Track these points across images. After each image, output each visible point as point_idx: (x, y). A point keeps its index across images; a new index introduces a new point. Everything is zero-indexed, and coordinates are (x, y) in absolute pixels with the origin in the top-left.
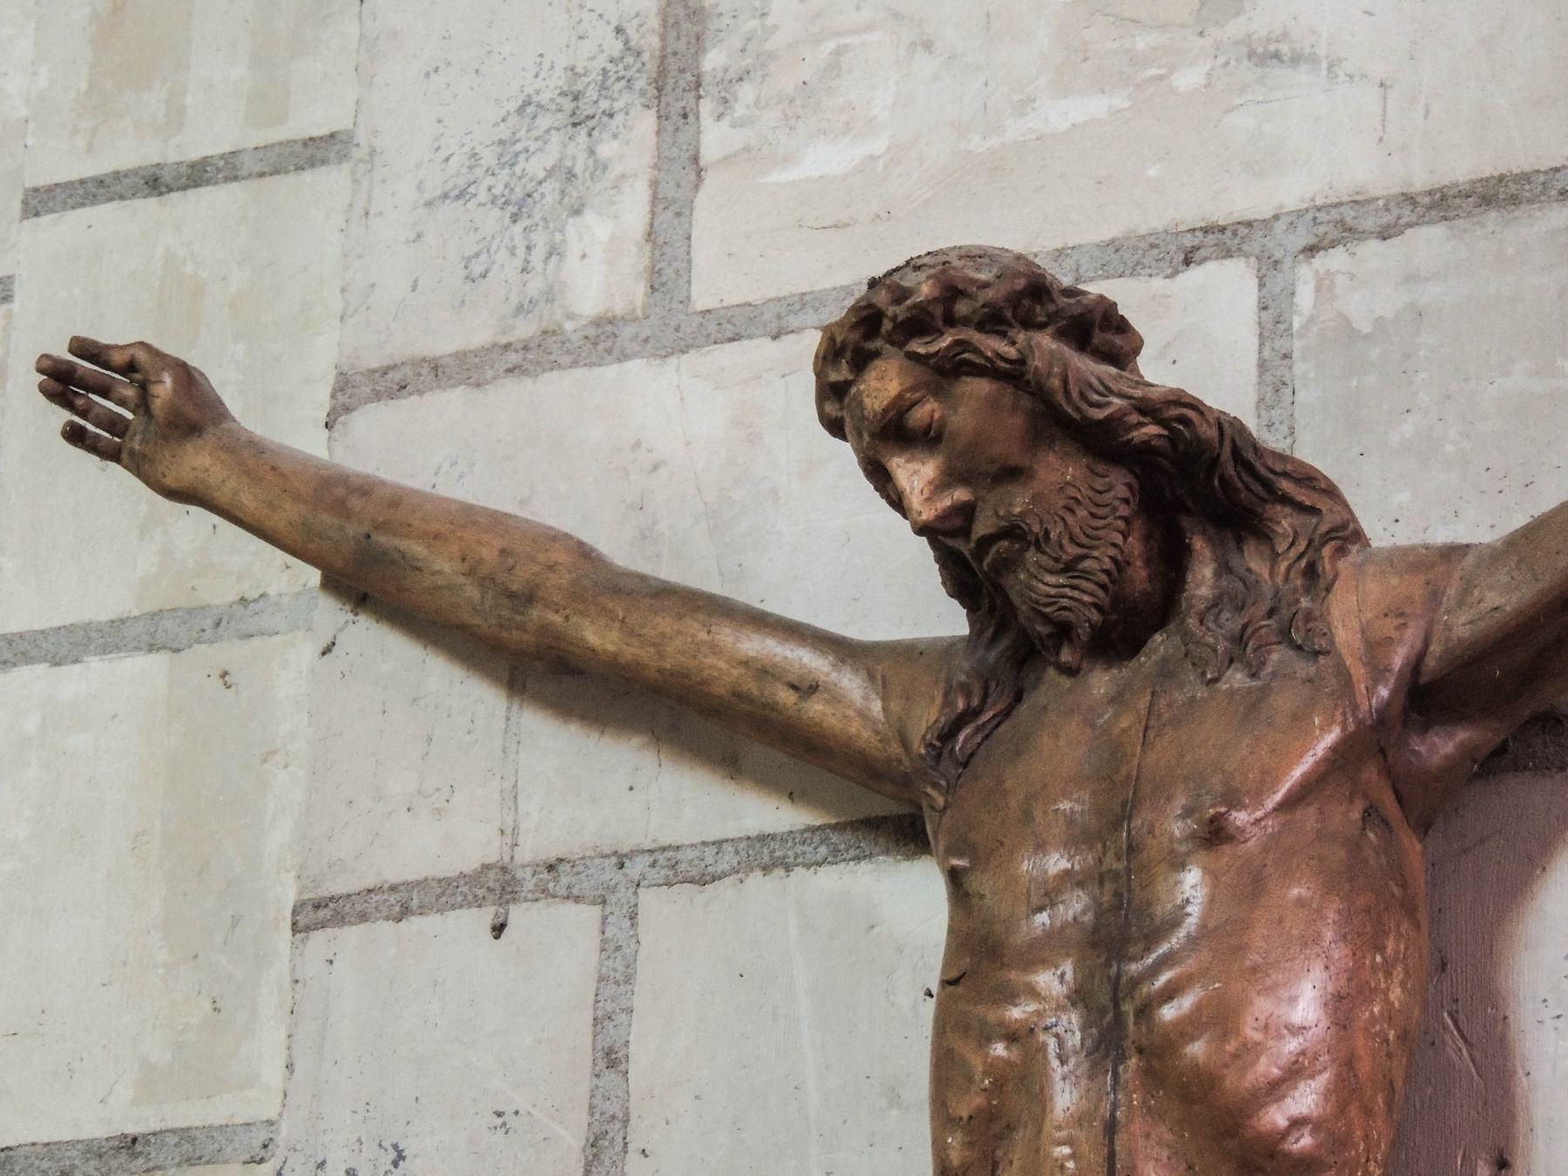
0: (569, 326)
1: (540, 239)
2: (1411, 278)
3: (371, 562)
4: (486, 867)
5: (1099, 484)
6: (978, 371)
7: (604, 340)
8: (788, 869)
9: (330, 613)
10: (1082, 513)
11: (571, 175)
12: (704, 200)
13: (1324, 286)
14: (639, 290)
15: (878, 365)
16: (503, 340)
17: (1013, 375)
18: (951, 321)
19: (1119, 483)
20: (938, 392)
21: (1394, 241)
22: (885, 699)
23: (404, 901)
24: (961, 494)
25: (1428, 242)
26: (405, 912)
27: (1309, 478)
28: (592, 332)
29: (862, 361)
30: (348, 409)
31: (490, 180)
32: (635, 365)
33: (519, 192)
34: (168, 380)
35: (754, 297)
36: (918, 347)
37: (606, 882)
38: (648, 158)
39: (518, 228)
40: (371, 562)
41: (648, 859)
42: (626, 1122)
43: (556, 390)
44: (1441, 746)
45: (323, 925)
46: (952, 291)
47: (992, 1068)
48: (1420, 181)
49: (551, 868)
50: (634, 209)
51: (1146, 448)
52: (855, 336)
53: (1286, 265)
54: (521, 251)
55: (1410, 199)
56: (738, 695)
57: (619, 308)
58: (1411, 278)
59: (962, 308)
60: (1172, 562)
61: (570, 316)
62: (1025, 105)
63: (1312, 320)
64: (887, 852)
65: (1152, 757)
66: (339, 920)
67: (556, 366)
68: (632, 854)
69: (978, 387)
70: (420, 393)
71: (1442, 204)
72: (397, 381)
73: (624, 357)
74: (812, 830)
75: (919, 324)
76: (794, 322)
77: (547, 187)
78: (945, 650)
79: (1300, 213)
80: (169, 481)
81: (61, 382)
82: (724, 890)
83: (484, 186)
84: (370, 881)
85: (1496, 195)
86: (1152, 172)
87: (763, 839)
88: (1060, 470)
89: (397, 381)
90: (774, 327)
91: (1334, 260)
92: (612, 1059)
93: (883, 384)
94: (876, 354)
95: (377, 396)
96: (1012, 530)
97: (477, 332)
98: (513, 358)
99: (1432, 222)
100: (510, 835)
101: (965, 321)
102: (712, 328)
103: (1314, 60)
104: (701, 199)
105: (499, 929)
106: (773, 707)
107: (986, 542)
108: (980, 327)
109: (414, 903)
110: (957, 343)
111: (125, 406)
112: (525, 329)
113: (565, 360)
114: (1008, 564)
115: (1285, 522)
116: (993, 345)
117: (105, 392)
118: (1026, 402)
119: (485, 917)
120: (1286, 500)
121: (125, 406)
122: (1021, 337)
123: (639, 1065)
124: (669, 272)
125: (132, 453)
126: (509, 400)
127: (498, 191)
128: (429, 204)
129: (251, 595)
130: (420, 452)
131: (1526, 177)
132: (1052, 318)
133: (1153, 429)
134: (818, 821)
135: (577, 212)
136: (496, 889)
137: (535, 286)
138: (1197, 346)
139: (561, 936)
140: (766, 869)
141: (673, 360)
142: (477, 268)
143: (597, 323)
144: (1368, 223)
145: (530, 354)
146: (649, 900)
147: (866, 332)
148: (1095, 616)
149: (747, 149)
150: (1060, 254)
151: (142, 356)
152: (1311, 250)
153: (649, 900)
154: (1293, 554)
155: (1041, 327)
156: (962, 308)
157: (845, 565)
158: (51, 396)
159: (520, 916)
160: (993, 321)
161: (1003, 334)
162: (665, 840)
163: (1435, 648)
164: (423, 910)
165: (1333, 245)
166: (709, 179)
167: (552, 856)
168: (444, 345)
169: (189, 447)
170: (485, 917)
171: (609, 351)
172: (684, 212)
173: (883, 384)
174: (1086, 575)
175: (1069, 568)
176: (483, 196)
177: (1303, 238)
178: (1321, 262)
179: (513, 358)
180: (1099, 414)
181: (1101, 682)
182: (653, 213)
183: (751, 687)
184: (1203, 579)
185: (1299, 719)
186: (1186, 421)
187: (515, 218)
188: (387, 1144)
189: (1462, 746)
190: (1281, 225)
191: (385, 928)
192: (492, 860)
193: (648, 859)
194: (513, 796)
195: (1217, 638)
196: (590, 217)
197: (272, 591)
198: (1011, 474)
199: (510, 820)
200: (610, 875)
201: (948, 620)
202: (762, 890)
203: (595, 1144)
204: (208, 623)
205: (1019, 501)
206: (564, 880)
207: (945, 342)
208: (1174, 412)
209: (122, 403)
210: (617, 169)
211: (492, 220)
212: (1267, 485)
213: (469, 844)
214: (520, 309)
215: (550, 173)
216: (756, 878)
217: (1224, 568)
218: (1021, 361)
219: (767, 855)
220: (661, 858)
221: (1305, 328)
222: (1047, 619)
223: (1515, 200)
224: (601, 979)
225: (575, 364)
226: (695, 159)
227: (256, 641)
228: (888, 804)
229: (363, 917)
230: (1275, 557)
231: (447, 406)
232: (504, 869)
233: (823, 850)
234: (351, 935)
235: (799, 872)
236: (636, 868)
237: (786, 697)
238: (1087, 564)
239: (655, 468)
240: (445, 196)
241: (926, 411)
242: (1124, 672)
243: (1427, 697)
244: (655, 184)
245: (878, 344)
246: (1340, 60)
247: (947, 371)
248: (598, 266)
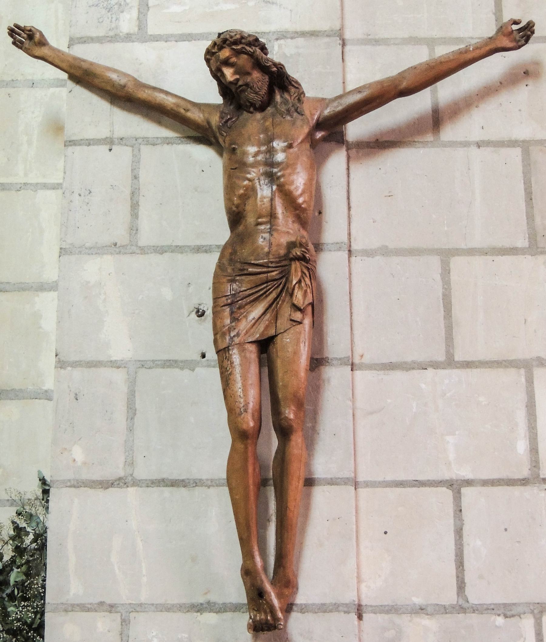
0: (121, 34)
1: (114, 16)
2: (297, 47)
3: (84, 76)
4: (107, 138)
5: (263, 78)
6: (246, 53)
7: (128, 38)
8: (172, 144)
9: (71, 84)
10: (260, 83)
11: (120, 5)
12: (149, 13)
13: (280, 46)
14: (136, 29)
15: (225, 49)
16: (107, 35)
17: (251, 55)
18: (241, 43)
19: (267, 78)
20: (236, 56)
21: (294, 40)
22: (203, 114)
23: (89, 143)
24: (238, 77)
25: (300, 41)
26: (89, 145)
27: (297, 82)
28: (126, 36)
29: (221, 48)
30: (73, 45)
31: (103, 4)
32: (136, 43)
33: (109, 7)
34: (38, 33)
35: (162, 33)
36: (234, 47)
37: (134, 143)
38: (137, 4)
39: (109, 14)
40: (84, 76)
41: (142, 140)
42: (139, 189)
43: (119, 46)
44: (319, 135)
45: (71, 145)
46: (242, 38)
47: (245, 186)
48: (299, 29)
49: (121, 139)
50: (135, 13)
51: (273, 72)
52: (221, 43)
53: (272, 41)
54: (110, 18)
55: (296, 32)
56: (172, 109)
57: (132, 32)
58: (297, 47)
59: (243, 41)
60: (271, 93)
61: (121, 32)
62: (218, 4)
63: (278, 52)
64: (193, 143)
65: (276, 130)
66: (75, 145)
67: (118, 42)
68: (139, 138)
69: (245, 56)
70: (88, 43)
71: (303, 34)
72: (84, 40)
73: (133, 42)
74: (177, 137)
75: (236, 43)
76: (169, 39)
77: (116, 6)
78: (218, 106)
79: (275, 32)
80: (36, 54)
81: (12, 32)
82: (158, 147)
83: (102, 5)
84: (82, 138)
85: (313, 34)
86: (244, 20)
87: (167, 138)
88: (256, 75)
89: (84, 40)
90: (165, 40)
91: (282, 42)
92: (136, 177)
93: (225, 53)
94: (225, 47)
95: (79, 43)
96: (247, 85)
97: (101, 33)
98: (109, 39)
99: (301, 37)
100: (112, 132)
101: (243, 44)
102: (152, 38)
103: (276, 4)
104: (149, 13)
105: (110, 150)
106: (179, 113)
107: (241, 86)
108: (247, 45)
109: (91, 143)
110: (243, 47)
111: (26, 39)
112: (111, 34)
113: (121, 41)
114: (243, 91)
115: (293, 90)
116: (248, 48)
117: (19, 35)
118: (252, 60)
119: (107, 147)
120: (293, 86)
121: (26, 39)
122: (254, 48)
123: (141, 180)
124: (143, 26)
125: (26, 48)
126: (108, 48)
127: (105, 6)
128: (90, 6)
129: (15, 79)
130: (90, 54)
131: (320, 32)
132: (259, 45)
133: (275, 69)
134: (180, 136)
135: (122, 12)
136: (110, 142)
137: (113, 25)
138: (277, 53)
139: (124, 154)
140: (168, 144)
141: (144, 44)
142: (101, 20)
143: (127, 34)
144: (288, 36)
145: (114, 39)
146: (142, 147)
147: (225, 41)
148: (260, 102)
149: (158, 5)
150: (496, 26)
151: (33, 29)
152: (277, 39)
153: (142, 147)
154: (295, 95)
155: (256, 46)
156: (243, 41)
157: (199, 88)
158: (9, 34)
159: (114, 148)
160: (250, 44)
161: (250, 47)
162: (145, 136)
163: (321, 117)
164: (93, 145)
165: (281, 39)
166: (151, 10)
167: (121, 137)
168: (94, 35)
169: (42, 48)
170: (108, 147)
171: (130, 40)
172: (145, 15)
173: (225, 53)
174: (259, 95)
175: (256, 93)
176: (101, 6)
177: (275, 37)
178: (279, 42)
179: (109, 39)
180: (268, 65)
181: (258, 116)
182: (139, 14)
183: (175, 109)
184: (278, 98)
185: (302, 126)
186: (281, 68)
187: (109, 11)
188: (87, 189)
189: (322, 136)
190: (271, 34)
191: (85, 148)
192: (108, 136)
193: (142, 140)
194: (112, 124)
195: (283, 108)
196: (125, 13)
197: (19, 79)
198: (249, 74)
199: (112, 129)
200: (134, 142)
201: (219, 100)
202: (166, 147)
203: (133, 193)
204: (5, 84)
205: (249, 79)
206: (124, 142)
207: (239, 47)
208: (280, 66)
209: (23, 38)
210: (130, 5)
211: (104, 11)
212: (290, 83)
213: (103, 132)
214: (110, 30)
215: (116, 4)
216: (165, 145)
217: (281, 97)
218: (254, 52)
219: (167, 141)
220: (145, 140)
221: (276, 54)
222: (250, 102)
223: (317, 36)
224: (133, 162)
225: (122, 42)
226: (147, 5)
227: (16, 89)
228: (203, 135)
229: (80, 145)
230: (291, 96)
231: (96, 46)
232: (111, 138)
233: (180, 141)
234: (78, 148)
235: (174, 145)
236: (140, 141)
237: (182, 111)
238: (260, 93)
239: (141, 64)
240: (93, 5)
241: (234, 60)
242: (263, 114)
243: (319, 125)
244: (139, 9)
245: (225, 45)
246: (282, 5)
247: (238, 53)
248: (127, 22)
